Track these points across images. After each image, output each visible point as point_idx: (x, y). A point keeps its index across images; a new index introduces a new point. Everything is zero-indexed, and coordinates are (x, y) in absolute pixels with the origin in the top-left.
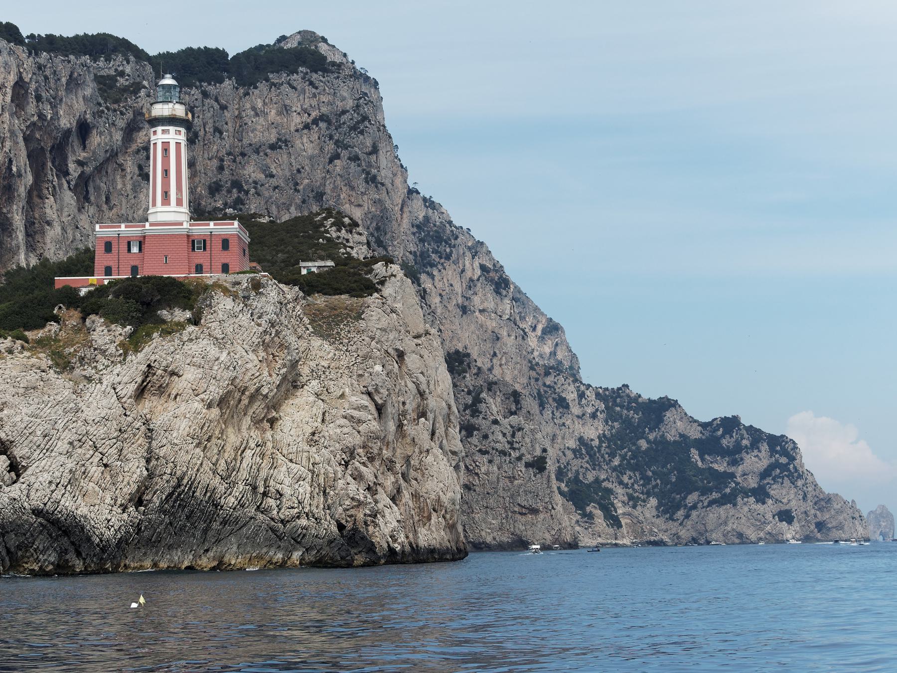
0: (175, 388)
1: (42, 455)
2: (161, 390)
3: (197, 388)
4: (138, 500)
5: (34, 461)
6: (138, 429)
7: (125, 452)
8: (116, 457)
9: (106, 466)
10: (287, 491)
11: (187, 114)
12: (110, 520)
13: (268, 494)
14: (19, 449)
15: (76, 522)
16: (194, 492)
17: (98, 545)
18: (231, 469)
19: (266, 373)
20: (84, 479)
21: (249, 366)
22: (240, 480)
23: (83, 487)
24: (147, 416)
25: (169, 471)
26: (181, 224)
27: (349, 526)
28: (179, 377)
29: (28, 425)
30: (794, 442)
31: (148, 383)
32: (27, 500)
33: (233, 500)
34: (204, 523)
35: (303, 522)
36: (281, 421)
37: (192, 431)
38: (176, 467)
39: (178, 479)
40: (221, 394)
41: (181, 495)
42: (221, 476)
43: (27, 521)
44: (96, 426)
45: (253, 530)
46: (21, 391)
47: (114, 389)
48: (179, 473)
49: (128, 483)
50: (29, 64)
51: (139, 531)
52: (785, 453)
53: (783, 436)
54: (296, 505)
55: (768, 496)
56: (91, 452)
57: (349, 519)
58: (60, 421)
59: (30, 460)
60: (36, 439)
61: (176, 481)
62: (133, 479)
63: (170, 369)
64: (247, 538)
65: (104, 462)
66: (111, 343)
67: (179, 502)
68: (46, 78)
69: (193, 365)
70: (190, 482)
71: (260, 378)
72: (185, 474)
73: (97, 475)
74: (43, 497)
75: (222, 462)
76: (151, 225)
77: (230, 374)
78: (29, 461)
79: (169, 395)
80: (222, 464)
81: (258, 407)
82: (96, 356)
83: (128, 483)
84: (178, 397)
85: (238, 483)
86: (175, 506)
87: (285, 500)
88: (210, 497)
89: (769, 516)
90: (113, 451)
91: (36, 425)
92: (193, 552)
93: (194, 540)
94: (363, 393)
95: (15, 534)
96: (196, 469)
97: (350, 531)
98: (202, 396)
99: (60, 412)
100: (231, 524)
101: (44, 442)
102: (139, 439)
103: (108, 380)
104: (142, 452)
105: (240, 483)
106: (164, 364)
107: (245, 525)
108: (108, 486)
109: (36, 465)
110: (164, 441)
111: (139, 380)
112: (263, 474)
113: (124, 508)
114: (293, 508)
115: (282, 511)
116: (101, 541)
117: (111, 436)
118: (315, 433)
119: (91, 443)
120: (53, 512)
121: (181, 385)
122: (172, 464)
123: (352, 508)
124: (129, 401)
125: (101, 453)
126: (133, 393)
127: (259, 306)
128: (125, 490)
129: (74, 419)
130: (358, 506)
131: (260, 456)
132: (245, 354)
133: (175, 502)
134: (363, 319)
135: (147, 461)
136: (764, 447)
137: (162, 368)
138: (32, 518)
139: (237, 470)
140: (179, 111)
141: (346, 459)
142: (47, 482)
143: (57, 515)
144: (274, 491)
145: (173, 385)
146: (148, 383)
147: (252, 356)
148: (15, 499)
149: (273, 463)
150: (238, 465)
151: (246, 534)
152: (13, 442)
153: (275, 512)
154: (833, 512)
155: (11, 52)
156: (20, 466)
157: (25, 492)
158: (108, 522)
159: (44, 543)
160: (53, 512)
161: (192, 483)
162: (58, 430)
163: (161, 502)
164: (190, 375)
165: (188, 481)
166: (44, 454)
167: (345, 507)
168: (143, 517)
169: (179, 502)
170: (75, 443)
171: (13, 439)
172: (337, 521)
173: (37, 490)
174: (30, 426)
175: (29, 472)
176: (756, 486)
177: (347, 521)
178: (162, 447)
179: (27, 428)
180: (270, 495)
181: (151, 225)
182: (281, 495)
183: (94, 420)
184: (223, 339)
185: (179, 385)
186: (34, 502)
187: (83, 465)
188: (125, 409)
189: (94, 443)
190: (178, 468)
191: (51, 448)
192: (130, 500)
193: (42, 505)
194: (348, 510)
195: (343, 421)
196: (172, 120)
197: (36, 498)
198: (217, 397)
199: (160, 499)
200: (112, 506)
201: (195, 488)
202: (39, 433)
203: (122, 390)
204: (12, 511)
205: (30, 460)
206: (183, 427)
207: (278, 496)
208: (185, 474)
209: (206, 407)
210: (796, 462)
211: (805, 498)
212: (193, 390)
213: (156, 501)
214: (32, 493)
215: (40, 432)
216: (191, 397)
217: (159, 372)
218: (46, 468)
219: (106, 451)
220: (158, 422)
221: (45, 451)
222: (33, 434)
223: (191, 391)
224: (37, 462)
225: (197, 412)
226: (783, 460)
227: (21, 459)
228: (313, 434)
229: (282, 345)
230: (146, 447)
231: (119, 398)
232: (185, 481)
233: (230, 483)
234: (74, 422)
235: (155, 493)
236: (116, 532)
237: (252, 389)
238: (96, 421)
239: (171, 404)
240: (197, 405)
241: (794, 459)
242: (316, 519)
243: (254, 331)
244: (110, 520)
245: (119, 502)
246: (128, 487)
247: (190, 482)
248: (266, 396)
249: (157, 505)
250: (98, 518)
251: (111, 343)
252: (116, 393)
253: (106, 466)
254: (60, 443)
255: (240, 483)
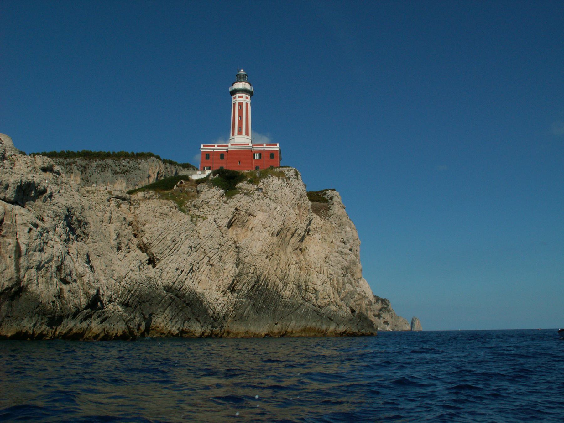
0: (252, 224)
1: (171, 253)
2: (243, 224)
3: (265, 224)
4: (232, 288)
5: (165, 256)
6: (230, 246)
7: (223, 258)
8: (218, 260)
9: (211, 265)
10: (320, 288)
11: (251, 89)
12: (218, 299)
13: (308, 290)
14: (155, 248)
15: (197, 298)
16: (267, 286)
17: (212, 316)
18: (284, 274)
19: (299, 222)
20: (199, 272)
21: (291, 216)
22: (290, 281)
23: (198, 277)
24: (235, 239)
25: (252, 271)
26: (248, 144)
27: (357, 311)
28: (254, 217)
29: (162, 233)
30: (389, 301)
31: (235, 220)
32: (160, 279)
33: (288, 293)
34: (274, 306)
35: (333, 308)
36: (307, 250)
37: (264, 248)
38: (256, 268)
39: (257, 276)
40: (278, 229)
41: (259, 287)
42: (279, 278)
43: (160, 294)
44: (205, 240)
45: (304, 311)
46: (158, 215)
47: (215, 221)
48: (258, 273)
49: (227, 277)
50: (163, 166)
51: (235, 308)
52: (386, 304)
53: (385, 299)
54: (327, 297)
55: (381, 317)
56: (203, 256)
57: (357, 307)
58: (183, 234)
59: (163, 255)
60: (167, 242)
61: (257, 278)
62: (231, 274)
63: (249, 212)
64: (301, 317)
65: (211, 263)
66: (212, 198)
67: (258, 292)
68: (168, 172)
69: (262, 211)
70: (265, 279)
71: (297, 224)
72: (262, 274)
73: (207, 271)
74: (172, 278)
75: (279, 270)
76: (231, 145)
77: (282, 218)
78: (161, 256)
79: (248, 228)
80: (279, 271)
81: (295, 239)
82: (203, 205)
83: (227, 277)
84: (253, 229)
85: (289, 283)
86: (256, 294)
87: (319, 294)
88: (276, 289)
89: (382, 323)
90: (216, 256)
91: (167, 234)
92: (268, 324)
93: (268, 317)
94: (341, 242)
95: (150, 304)
96: (267, 272)
97: (358, 314)
98: (268, 228)
99: (183, 229)
100: (289, 307)
101: (173, 245)
102: (231, 252)
103: (210, 218)
104: (233, 260)
105: (290, 283)
106: (246, 208)
107: (298, 309)
108: (214, 278)
109: (167, 258)
110: (247, 253)
111: (230, 217)
112: (303, 278)
113: (225, 293)
114: (325, 298)
115: (319, 300)
116: (214, 313)
117: (215, 247)
118: (326, 258)
119: (203, 250)
120: (180, 289)
121: (255, 222)
122: (254, 267)
123: (359, 300)
124: (224, 228)
125: (208, 257)
126: (227, 224)
127: (295, 184)
128: (225, 281)
129: (192, 234)
130: (362, 299)
131: (299, 268)
132: (289, 209)
133: (256, 291)
134: (331, 209)
135: (236, 266)
136: (380, 302)
137: (244, 211)
138: (163, 292)
139: (287, 275)
140: (248, 86)
141: (344, 273)
142: (175, 268)
143: (182, 291)
144: (312, 288)
145: (250, 222)
146: (235, 220)
147: (292, 211)
148: (151, 278)
149: (307, 273)
150: (288, 272)
151: (300, 314)
152: (151, 243)
153: (314, 301)
154: (400, 322)
155: (157, 162)
156: (156, 259)
157: (159, 274)
158: (217, 300)
159: (172, 312)
160: (180, 289)
161: (266, 280)
162: (182, 239)
163: (248, 291)
164: (260, 216)
165: (264, 279)
166: (173, 252)
167: (355, 299)
168: (238, 299)
169: (258, 292)
170: (193, 249)
171: (151, 242)
172: (350, 308)
173: (168, 272)
174: (163, 233)
175: (162, 262)
176: (377, 314)
177: (356, 308)
178: (246, 257)
179: (161, 235)
180: (309, 291)
181: (231, 145)
182: (316, 291)
183: (204, 236)
184: (276, 200)
185: (254, 222)
186: (165, 281)
187: (198, 263)
188: (222, 233)
189: (205, 250)
190: (258, 269)
191: (177, 249)
192: (229, 288)
193: (172, 284)
194: (357, 301)
195: (337, 254)
196: (244, 91)
197: (167, 278)
198: (276, 231)
199: (247, 289)
200: (217, 291)
201: (268, 283)
202: (169, 239)
203: (220, 222)
204: (148, 286)
205: (163, 255)
206: (257, 247)
207: (314, 292)
208: (262, 274)
209: (270, 235)
210: (389, 307)
211: (392, 317)
212: (263, 225)
213: (245, 290)
214: (164, 274)
215: (170, 238)
216: (261, 229)
217: (243, 213)
218: (174, 260)
219: (212, 255)
220: (241, 243)
221: (173, 250)
222: (165, 239)
223: (261, 225)
224: (168, 257)
225: (265, 237)
226: (386, 306)
227: (157, 254)
228: (326, 258)
229: (306, 208)
230: (235, 257)
231: (218, 227)
232: (262, 278)
233: (284, 283)
234: (191, 236)
235: (244, 285)
236: (223, 308)
237: (293, 229)
238: (205, 237)
239: (249, 233)
240: (265, 234)
241: (389, 306)
242: (339, 306)
243: (293, 197)
244: (218, 299)
245: (221, 289)
246: (227, 279)
247: (265, 279)
248: (300, 235)
249: (246, 292)
250: (210, 297)
251: (212, 198)
252: (217, 224)
253: (211, 265)
254: (183, 247)
255: (290, 283)
